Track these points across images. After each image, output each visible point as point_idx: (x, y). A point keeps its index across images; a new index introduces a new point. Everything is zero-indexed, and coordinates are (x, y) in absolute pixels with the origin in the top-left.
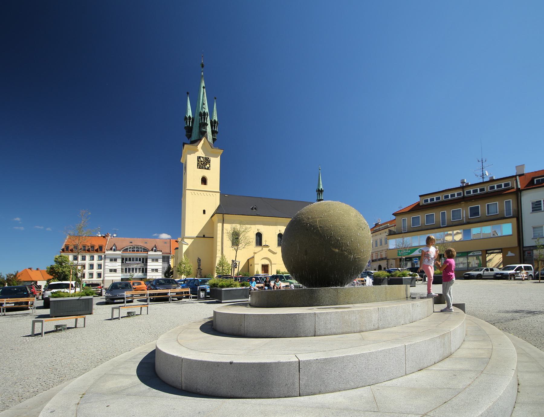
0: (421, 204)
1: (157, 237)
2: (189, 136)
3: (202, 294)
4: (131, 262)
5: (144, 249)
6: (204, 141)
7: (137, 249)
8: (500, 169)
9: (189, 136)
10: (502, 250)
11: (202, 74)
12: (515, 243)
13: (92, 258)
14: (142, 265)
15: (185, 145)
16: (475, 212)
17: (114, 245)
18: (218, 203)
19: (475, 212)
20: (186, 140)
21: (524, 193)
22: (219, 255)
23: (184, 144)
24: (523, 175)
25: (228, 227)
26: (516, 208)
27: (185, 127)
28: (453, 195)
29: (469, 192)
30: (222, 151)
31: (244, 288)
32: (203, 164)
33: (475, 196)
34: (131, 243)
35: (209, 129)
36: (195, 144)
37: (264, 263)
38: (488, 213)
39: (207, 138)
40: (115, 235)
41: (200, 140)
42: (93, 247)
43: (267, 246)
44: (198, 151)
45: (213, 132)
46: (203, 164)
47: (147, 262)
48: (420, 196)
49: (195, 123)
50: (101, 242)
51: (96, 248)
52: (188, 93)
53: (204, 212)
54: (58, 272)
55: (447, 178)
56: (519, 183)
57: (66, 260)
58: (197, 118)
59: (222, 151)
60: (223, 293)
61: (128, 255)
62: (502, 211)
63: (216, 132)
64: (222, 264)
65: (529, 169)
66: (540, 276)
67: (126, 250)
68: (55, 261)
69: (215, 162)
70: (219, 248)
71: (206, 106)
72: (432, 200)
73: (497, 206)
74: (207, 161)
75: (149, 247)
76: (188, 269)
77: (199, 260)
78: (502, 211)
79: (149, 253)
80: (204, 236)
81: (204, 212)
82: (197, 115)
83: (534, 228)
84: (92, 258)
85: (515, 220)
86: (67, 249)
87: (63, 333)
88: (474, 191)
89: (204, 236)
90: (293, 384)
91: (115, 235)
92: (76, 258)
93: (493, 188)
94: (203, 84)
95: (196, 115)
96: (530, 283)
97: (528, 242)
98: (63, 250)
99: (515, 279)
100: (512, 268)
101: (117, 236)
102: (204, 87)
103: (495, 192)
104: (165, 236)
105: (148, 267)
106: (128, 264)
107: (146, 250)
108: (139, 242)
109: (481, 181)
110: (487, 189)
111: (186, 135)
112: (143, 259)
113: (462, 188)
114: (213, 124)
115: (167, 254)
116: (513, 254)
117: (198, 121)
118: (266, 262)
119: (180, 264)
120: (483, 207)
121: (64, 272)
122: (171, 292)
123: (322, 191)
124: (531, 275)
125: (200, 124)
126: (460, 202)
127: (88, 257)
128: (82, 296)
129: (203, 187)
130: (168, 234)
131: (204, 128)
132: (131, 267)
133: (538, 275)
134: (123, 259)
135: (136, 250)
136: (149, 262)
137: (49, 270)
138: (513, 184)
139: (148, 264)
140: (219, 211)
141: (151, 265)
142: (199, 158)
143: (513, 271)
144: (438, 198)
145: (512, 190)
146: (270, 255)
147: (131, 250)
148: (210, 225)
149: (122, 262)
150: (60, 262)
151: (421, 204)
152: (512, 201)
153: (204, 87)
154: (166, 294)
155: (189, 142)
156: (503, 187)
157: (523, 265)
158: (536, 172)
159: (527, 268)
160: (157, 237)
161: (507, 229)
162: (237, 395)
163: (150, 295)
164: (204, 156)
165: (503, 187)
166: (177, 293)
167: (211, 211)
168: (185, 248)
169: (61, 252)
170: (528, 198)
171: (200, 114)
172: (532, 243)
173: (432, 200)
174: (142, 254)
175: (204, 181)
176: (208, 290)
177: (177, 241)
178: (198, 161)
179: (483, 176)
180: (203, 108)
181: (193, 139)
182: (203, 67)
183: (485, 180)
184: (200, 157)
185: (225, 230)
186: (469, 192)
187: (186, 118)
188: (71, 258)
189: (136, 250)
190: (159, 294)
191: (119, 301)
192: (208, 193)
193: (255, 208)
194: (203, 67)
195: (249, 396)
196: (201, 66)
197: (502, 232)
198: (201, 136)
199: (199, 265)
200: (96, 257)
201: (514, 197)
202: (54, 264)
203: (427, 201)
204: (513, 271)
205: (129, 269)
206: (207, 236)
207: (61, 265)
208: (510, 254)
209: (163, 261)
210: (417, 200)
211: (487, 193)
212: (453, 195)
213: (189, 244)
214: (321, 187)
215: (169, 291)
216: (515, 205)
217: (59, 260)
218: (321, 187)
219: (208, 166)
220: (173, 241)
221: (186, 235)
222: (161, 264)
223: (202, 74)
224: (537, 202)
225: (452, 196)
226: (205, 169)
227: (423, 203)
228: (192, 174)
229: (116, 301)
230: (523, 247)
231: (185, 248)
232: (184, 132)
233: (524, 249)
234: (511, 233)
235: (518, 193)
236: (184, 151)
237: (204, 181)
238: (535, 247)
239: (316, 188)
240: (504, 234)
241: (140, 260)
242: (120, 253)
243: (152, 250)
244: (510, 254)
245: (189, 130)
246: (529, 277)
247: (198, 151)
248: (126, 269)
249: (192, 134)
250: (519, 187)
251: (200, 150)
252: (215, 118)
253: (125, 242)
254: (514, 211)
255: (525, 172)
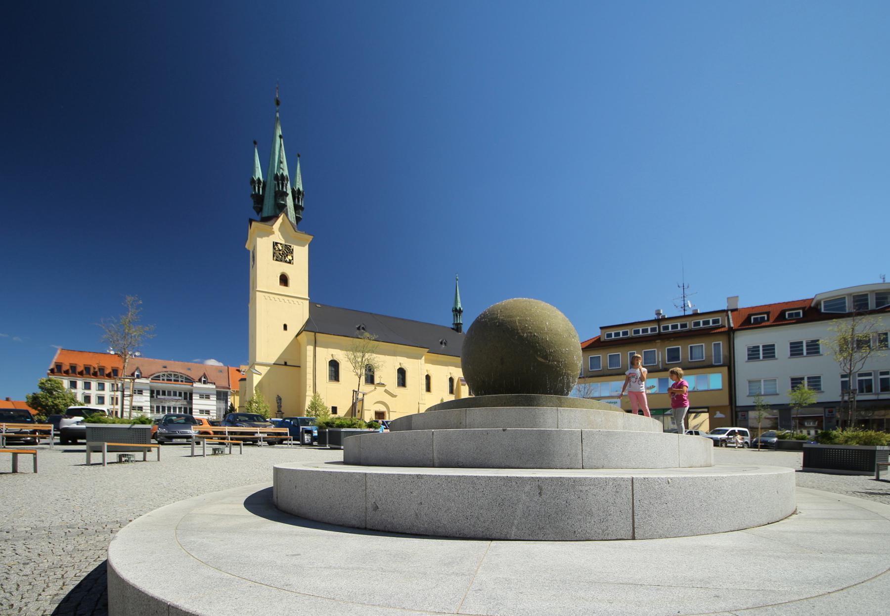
0: (602, 340)
1: (202, 363)
2: (259, 210)
3: (307, 438)
4: (166, 397)
5: (186, 379)
6: (283, 220)
7: (177, 378)
8: (707, 300)
9: (259, 210)
10: (709, 409)
11: (278, 115)
12: (726, 402)
13: (101, 387)
14: (185, 403)
15: (253, 223)
16: (674, 355)
17: (137, 369)
18: (306, 316)
19: (674, 355)
20: (254, 215)
21: (737, 334)
22: (310, 393)
23: (251, 221)
24: (736, 310)
25: (325, 355)
26: (727, 354)
27: (252, 195)
28: (645, 331)
29: (667, 328)
30: (310, 238)
31: (372, 430)
32: (283, 254)
33: (675, 333)
34: (165, 367)
35: (289, 201)
36: (270, 223)
37: (378, 410)
38: (691, 358)
39: (287, 215)
40: (137, 354)
41: (277, 217)
42: (102, 369)
43: (383, 385)
44: (273, 233)
45: (297, 208)
46: (283, 254)
47: (191, 399)
48: (601, 328)
49: (267, 189)
50: (117, 364)
51: (107, 372)
52: (255, 143)
53: (285, 327)
54: (47, 405)
55: (637, 308)
56: (731, 321)
57: (59, 387)
58: (271, 183)
59: (310, 238)
60: (342, 435)
61: (160, 385)
62: (709, 357)
63: (302, 208)
64: (314, 406)
65: (746, 302)
66: (759, 444)
67: (157, 378)
68: (40, 387)
69: (301, 254)
70: (310, 382)
71: (285, 165)
72: (617, 334)
73: (703, 349)
74: (288, 250)
75: (194, 375)
76: (263, 410)
77: (279, 399)
78: (709, 357)
79: (195, 385)
80: (286, 364)
81: (285, 327)
82: (270, 178)
83: (750, 382)
84: (101, 387)
85: (725, 369)
86: (58, 369)
87: (130, 464)
88: (673, 327)
89: (286, 364)
90: (576, 455)
91: (137, 354)
92: (73, 385)
93: (697, 324)
94: (279, 132)
95: (269, 178)
96: (747, 451)
97: (743, 399)
98: (52, 371)
99: (727, 446)
100: (724, 432)
101: (140, 356)
102: (281, 137)
103: (701, 330)
104: (212, 362)
105: (194, 407)
106: (161, 401)
107: (190, 381)
108: (177, 367)
109: (682, 314)
110: (690, 325)
111: (254, 208)
112: (185, 394)
113: (658, 321)
114: (296, 194)
115: (224, 388)
116: (722, 416)
117: (273, 187)
118: (382, 408)
119: (250, 403)
120: (684, 349)
121: (57, 405)
122: (260, 431)
123: (460, 311)
124: (746, 443)
125: (275, 192)
126: (655, 340)
127: (94, 384)
128: (135, 423)
129: (283, 289)
130: (219, 361)
131: (283, 200)
132: (166, 405)
133: (757, 442)
134: (152, 392)
135: (173, 378)
136: (196, 399)
137: (30, 400)
138: (723, 320)
139: (194, 402)
140: (308, 327)
141: (198, 404)
142: (275, 244)
143: (724, 436)
144: (625, 333)
145: (723, 330)
146: (387, 399)
147: (165, 378)
148: (295, 347)
149: (152, 397)
150: (50, 390)
151: (602, 340)
152: (722, 343)
153: (281, 137)
154: (253, 433)
155: (259, 219)
156: (711, 324)
157: (737, 429)
158: (753, 308)
159: (743, 433)
160: (202, 363)
161: (716, 381)
162: (513, 465)
163: (231, 433)
164: (283, 242)
165: (711, 324)
166: (269, 434)
167: (296, 326)
168: (257, 379)
169: (48, 374)
170: (744, 341)
171: (276, 177)
172: (750, 402)
173: (617, 334)
174: (186, 387)
175: (284, 280)
176: (315, 433)
177: (239, 371)
178: (274, 248)
179: (684, 307)
180: (279, 168)
181: (265, 214)
182: (278, 103)
183: (687, 313)
184: (277, 243)
185: (318, 357)
186: (666, 328)
187: (253, 181)
188: (66, 383)
189: (173, 378)
190: (242, 433)
191: (179, 440)
192: (295, 300)
193: (363, 329)
194: (278, 103)
195: (527, 466)
196: (275, 103)
197: (708, 385)
198: (278, 211)
199: (279, 406)
200: (108, 385)
201: (725, 338)
202: (39, 392)
203: (610, 335)
204: (724, 436)
205: (164, 408)
206: (290, 364)
207: (51, 393)
208: (719, 415)
209: (217, 399)
210: (597, 333)
211: (690, 331)
212: (645, 331)
213: (263, 374)
214: (459, 305)
215: (258, 430)
216: (727, 350)
217: (48, 386)
218: (459, 305)
219: (290, 257)
220: (232, 369)
221: (258, 360)
222: (215, 403)
223: (278, 115)
224: (754, 347)
225: (644, 331)
226: (286, 262)
227: (604, 338)
228: (266, 269)
229: (175, 441)
230: (736, 407)
231: (257, 379)
232: (251, 203)
233: (738, 409)
234: (720, 387)
235: (730, 333)
236: (250, 231)
237: (284, 280)
238: (752, 408)
239: (452, 306)
240: (711, 388)
241: (180, 395)
242: (147, 381)
243: (200, 381)
244: (719, 415)
245: (259, 200)
246: (745, 445)
247: (273, 233)
248: (158, 408)
249: (264, 206)
250: (732, 325)
251: (277, 233)
252: (299, 186)
253: (156, 365)
254: (725, 357)
255: (740, 306)
